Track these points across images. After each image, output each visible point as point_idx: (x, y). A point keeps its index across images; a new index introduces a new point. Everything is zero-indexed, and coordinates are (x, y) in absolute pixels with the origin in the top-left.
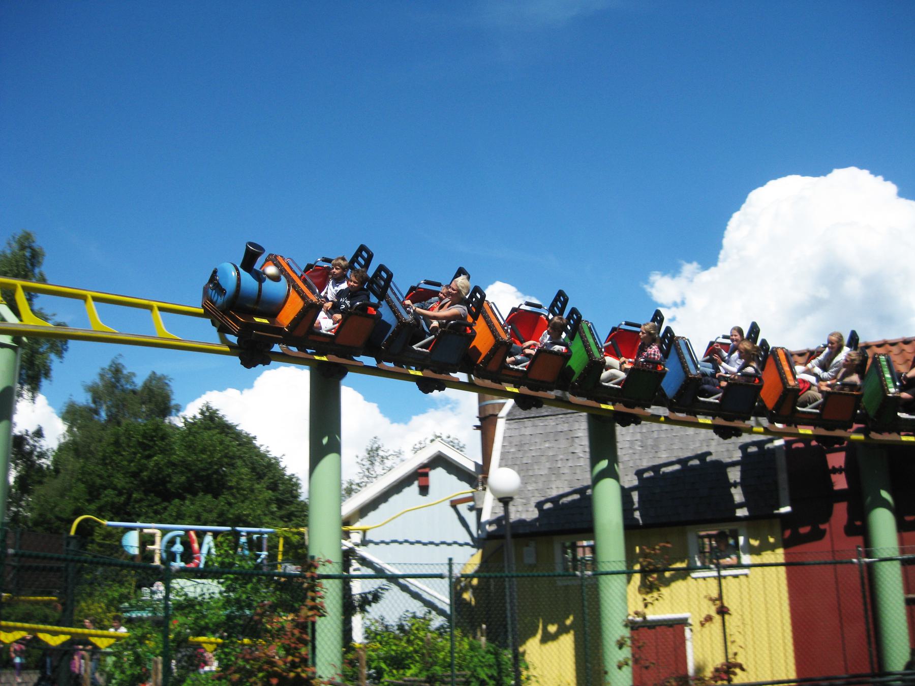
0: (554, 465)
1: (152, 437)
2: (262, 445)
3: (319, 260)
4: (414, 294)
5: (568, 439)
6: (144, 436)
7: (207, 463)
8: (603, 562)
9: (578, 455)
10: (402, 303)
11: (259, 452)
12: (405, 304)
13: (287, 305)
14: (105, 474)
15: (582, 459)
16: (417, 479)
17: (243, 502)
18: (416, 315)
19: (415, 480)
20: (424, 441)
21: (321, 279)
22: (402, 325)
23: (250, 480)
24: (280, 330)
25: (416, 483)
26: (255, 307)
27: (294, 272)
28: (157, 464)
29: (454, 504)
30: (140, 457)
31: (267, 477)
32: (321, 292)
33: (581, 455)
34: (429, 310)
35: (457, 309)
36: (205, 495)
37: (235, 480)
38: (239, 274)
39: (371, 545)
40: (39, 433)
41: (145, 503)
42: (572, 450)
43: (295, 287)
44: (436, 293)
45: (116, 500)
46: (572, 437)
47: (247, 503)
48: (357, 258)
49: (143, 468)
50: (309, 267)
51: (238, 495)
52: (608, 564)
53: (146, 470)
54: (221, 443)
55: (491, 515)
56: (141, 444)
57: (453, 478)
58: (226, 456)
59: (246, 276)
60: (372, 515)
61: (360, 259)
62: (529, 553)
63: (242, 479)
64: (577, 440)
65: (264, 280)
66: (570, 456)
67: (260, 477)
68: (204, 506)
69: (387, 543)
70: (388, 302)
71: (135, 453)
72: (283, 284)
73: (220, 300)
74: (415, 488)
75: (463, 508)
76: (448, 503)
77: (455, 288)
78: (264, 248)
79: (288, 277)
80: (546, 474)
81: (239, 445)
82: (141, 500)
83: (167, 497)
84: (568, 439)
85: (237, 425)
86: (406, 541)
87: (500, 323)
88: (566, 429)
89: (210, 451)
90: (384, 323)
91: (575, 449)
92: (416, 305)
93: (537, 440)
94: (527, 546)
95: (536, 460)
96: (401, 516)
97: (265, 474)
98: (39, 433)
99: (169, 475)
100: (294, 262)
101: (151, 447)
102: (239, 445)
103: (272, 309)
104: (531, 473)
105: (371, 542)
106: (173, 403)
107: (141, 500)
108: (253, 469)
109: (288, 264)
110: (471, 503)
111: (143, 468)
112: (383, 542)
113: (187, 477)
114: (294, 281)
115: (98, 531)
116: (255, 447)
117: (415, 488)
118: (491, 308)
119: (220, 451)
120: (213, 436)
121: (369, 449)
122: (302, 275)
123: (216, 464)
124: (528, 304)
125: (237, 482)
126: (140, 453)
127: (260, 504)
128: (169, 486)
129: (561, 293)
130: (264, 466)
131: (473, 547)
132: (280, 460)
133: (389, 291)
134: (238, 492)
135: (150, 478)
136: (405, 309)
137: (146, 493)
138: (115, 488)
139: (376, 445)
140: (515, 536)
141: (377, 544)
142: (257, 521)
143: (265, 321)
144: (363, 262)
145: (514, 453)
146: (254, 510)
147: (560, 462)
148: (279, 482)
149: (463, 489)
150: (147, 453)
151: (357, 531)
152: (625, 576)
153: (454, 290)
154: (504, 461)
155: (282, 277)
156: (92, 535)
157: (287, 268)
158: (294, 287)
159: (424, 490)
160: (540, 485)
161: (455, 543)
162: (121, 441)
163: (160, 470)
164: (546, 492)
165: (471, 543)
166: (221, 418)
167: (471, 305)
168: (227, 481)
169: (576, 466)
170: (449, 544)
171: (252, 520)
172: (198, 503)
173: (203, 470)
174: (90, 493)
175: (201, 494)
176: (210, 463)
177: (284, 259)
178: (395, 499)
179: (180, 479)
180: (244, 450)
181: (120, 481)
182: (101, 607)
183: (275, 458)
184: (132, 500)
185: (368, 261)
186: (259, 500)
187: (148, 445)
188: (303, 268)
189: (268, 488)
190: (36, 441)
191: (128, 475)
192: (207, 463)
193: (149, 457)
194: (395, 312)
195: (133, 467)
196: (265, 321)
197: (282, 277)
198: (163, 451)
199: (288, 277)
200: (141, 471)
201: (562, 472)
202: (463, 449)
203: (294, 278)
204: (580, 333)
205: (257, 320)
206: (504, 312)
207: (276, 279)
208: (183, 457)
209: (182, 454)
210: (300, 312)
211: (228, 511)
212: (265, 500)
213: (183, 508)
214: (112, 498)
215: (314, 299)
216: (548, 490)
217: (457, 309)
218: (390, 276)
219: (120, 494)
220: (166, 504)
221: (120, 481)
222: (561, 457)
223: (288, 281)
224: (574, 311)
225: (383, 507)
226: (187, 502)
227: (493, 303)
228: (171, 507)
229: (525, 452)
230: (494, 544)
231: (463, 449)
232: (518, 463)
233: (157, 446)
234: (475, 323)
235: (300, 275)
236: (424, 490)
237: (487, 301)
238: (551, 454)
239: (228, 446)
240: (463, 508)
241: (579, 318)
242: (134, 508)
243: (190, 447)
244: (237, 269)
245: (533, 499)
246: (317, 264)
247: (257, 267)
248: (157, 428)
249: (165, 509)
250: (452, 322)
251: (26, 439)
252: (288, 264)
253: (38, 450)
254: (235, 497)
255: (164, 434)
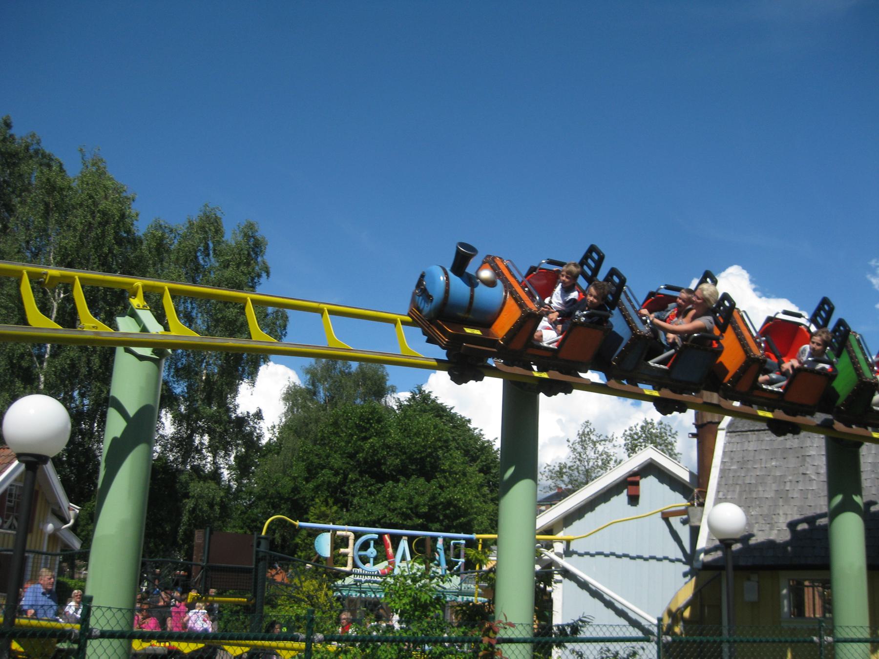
0: (782, 487)
1: (369, 420)
2: (475, 429)
3: (544, 261)
4: (653, 300)
5: (798, 457)
6: (361, 418)
7: (421, 446)
8: (841, 627)
9: (810, 477)
10: (637, 312)
11: (473, 434)
12: (640, 313)
13: (503, 314)
14: (324, 454)
15: (815, 482)
16: (626, 487)
17: (455, 486)
18: (655, 329)
19: (624, 489)
20: (635, 427)
21: (545, 282)
22: (637, 338)
23: (463, 463)
24: (494, 343)
25: (625, 491)
26: (466, 316)
27: (513, 276)
28: (372, 446)
29: (666, 516)
30: (356, 438)
31: (479, 460)
32: (543, 298)
33: (813, 477)
34: (665, 321)
35: (704, 321)
36: (418, 477)
37: (448, 463)
38: (448, 278)
39: (575, 556)
40: (259, 415)
41: (359, 484)
42: (802, 470)
43: (513, 294)
44: (673, 299)
45: (332, 480)
46: (803, 456)
47: (459, 487)
48: (587, 260)
49: (360, 450)
50: (532, 269)
51: (450, 479)
52: (847, 630)
53: (363, 452)
54: (435, 427)
55: (708, 542)
56: (358, 426)
57: (666, 488)
58: (439, 440)
59: (456, 281)
60: (577, 524)
61: (590, 261)
62: (750, 589)
63: (455, 463)
64: (808, 459)
65: (476, 285)
66: (801, 478)
67: (474, 459)
68: (416, 489)
69: (592, 555)
70: (621, 311)
71: (352, 435)
72: (498, 292)
73: (427, 308)
74: (623, 497)
75: (675, 521)
76: (659, 515)
77: (700, 296)
78: (477, 249)
79: (505, 281)
80: (772, 498)
81: (454, 427)
82: (357, 480)
83: (382, 478)
84: (798, 457)
85: (452, 408)
86: (613, 554)
87: (752, 335)
88: (795, 446)
89: (424, 434)
90: (615, 334)
91: (807, 469)
92: (653, 315)
93: (763, 457)
94: (749, 579)
95: (761, 480)
96: (609, 527)
97: (478, 457)
98: (259, 415)
99: (384, 457)
100: (513, 265)
101: (367, 430)
102: (454, 427)
103: (486, 320)
104: (754, 496)
105: (576, 553)
106: (389, 384)
107: (357, 480)
108: (467, 453)
109: (507, 267)
110: (685, 517)
111: (360, 450)
112: (587, 554)
113: (401, 460)
114: (511, 286)
115: (313, 511)
116: (469, 429)
117: (623, 497)
118: (742, 317)
119: (434, 435)
120: (426, 420)
121: (581, 432)
122: (522, 281)
123: (430, 447)
124: (786, 313)
125: (450, 466)
126: (356, 434)
127: (471, 488)
128: (383, 468)
129: (825, 301)
130: (476, 448)
131: (684, 563)
132: (493, 443)
133: (623, 296)
134: (450, 475)
135: (365, 459)
136: (640, 318)
137: (361, 473)
138: (331, 469)
139: (587, 430)
140: (737, 568)
141: (581, 555)
142: (468, 506)
143: (477, 332)
144: (593, 265)
145: (735, 471)
146: (465, 495)
147: (788, 484)
148: (492, 465)
149: (678, 501)
150: (363, 435)
151: (561, 541)
152: (868, 645)
153: (699, 299)
154: (723, 479)
155: (499, 282)
156: (307, 513)
157: (506, 272)
158: (511, 294)
159: (634, 500)
160: (765, 511)
161: (666, 558)
162: (339, 422)
163: (375, 452)
164: (772, 518)
165: (684, 560)
166: (434, 401)
167: (718, 315)
168: (439, 464)
169: (807, 490)
170: (659, 560)
171: (462, 505)
172: (411, 486)
173: (417, 452)
174: (309, 471)
175: (413, 477)
176: (424, 447)
177: (503, 261)
178: (602, 508)
179: (394, 461)
180: (458, 432)
181: (337, 461)
182: (313, 585)
183: (488, 441)
184: (348, 481)
185: (599, 263)
186: (470, 484)
187: (364, 427)
188: (524, 272)
189: (480, 471)
190: (256, 423)
191: (345, 456)
192: (421, 446)
193: (365, 439)
194: (629, 322)
195: (350, 450)
196: (477, 332)
197: (499, 282)
198: (378, 434)
199: (505, 281)
200: (357, 452)
201: (790, 496)
202: (675, 436)
203: (512, 283)
204: (849, 353)
205: (468, 331)
206: (757, 322)
207: (490, 284)
208: (398, 440)
209: (397, 438)
210: (517, 322)
211: (440, 494)
212: (477, 484)
213: (397, 490)
214: (329, 477)
215: (533, 307)
216: (774, 516)
217: (704, 321)
218: (623, 281)
219: (336, 474)
220: (380, 485)
221: (337, 461)
222: (790, 478)
223: (505, 287)
224: (841, 323)
225: (589, 516)
226: (400, 485)
227: (745, 312)
228: (385, 488)
229: (748, 470)
230: (709, 575)
231: (675, 436)
232: (740, 482)
233: (373, 428)
234: (723, 336)
235: (520, 281)
236: (634, 500)
237: (737, 309)
238: (778, 474)
239: (443, 430)
240: (675, 521)
241: (848, 331)
242: (349, 488)
243: (405, 430)
244: (446, 273)
245: (757, 525)
246: (542, 267)
247: (470, 269)
248: (374, 411)
249: (379, 489)
250: (695, 335)
251: (247, 421)
252: (507, 267)
253: (258, 431)
254: (447, 481)
255: (381, 417)
